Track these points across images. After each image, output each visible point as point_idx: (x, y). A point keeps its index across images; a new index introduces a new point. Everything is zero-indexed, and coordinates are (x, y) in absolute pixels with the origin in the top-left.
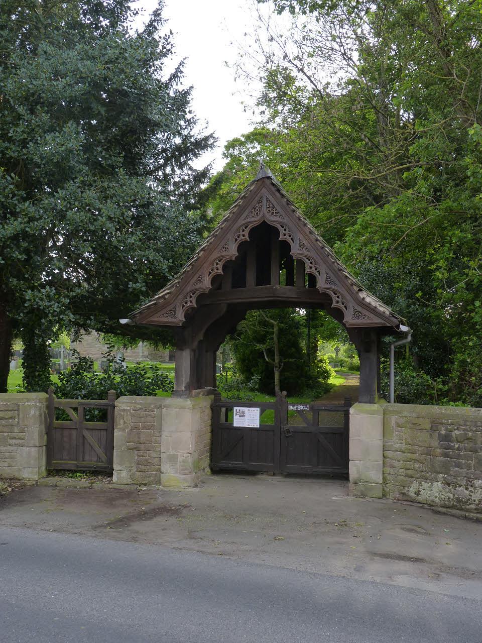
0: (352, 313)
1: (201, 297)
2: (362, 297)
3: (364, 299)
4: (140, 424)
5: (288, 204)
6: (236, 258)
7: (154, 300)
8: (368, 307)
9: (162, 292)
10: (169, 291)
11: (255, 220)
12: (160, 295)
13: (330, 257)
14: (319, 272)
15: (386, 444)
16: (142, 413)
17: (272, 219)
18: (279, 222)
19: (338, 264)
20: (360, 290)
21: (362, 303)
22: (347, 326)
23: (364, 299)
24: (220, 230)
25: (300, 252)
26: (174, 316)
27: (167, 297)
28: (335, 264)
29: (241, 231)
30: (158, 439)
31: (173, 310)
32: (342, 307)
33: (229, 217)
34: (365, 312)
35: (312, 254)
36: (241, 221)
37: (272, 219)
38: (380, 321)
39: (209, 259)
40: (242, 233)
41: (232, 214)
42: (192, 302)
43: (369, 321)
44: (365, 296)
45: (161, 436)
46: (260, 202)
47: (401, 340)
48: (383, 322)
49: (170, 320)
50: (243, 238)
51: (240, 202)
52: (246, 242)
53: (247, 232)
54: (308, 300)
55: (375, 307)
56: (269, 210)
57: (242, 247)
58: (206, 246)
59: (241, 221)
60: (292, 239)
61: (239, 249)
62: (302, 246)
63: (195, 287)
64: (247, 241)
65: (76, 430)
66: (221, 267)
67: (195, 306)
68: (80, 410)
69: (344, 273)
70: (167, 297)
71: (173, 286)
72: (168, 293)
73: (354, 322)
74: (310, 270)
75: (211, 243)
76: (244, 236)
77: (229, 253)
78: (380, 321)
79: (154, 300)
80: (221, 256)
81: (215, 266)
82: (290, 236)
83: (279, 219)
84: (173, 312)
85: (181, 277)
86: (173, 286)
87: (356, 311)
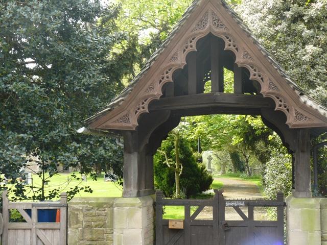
0: (294, 115)
1: (153, 103)
2: (304, 101)
3: (305, 102)
4: (93, 223)
5: (233, 17)
6: (136, 128)
7: (109, 107)
8: (310, 110)
9: (117, 99)
10: (123, 98)
11: (203, 32)
12: (115, 102)
13: (273, 64)
14: (262, 79)
15: (324, 235)
16: (93, 212)
17: (217, 30)
18: (224, 34)
19: (281, 71)
20: (302, 94)
21: (304, 106)
22: (290, 127)
23: (305, 102)
24: (170, 42)
25: (245, 60)
26: (128, 121)
27: (120, 104)
28: (278, 71)
29: (189, 42)
30: (110, 236)
31: (127, 116)
32: (285, 110)
33: (177, 29)
34: (305, 114)
35: (258, 63)
36: (189, 34)
37: (217, 31)
38: (320, 122)
39: (161, 67)
40: (166, 75)
41: (180, 27)
42: (169, 78)
43: (310, 122)
44: (306, 99)
45: (113, 233)
46: (206, 15)
47: (257, 200)
48: (323, 122)
49: (124, 124)
50: (191, 48)
51: (188, 15)
52: (194, 52)
53: (194, 43)
54: (247, 106)
55: (317, 110)
56: (215, 23)
57: (189, 57)
58: (157, 56)
59: (189, 34)
60: (237, 49)
61: (139, 121)
62: (246, 55)
63: (147, 94)
64: (147, 113)
65: (29, 231)
66: (147, 106)
67: (196, 50)
68: (34, 213)
69: (286, 78)
70: (120, 104)
71: (126, 94)
72: (123, 100)
73: (298, 122)
74: (254, 77)
75: (161, 54)
76: (143, 108)
77: (179, 63)
78: (320, 122)
79: (109, 107)
80: (170, 66)
81: (189, 44)
82: (234, 46)
83: (225, 31)
84: (126, 118)
85: (135, 85)
86: (126, 94)
87: (297, 113)
